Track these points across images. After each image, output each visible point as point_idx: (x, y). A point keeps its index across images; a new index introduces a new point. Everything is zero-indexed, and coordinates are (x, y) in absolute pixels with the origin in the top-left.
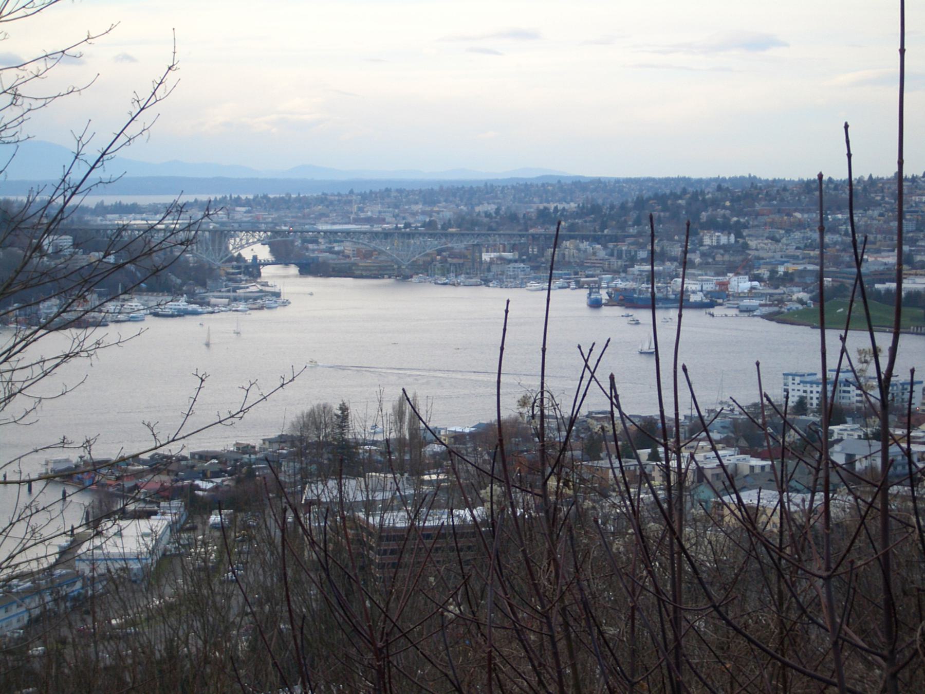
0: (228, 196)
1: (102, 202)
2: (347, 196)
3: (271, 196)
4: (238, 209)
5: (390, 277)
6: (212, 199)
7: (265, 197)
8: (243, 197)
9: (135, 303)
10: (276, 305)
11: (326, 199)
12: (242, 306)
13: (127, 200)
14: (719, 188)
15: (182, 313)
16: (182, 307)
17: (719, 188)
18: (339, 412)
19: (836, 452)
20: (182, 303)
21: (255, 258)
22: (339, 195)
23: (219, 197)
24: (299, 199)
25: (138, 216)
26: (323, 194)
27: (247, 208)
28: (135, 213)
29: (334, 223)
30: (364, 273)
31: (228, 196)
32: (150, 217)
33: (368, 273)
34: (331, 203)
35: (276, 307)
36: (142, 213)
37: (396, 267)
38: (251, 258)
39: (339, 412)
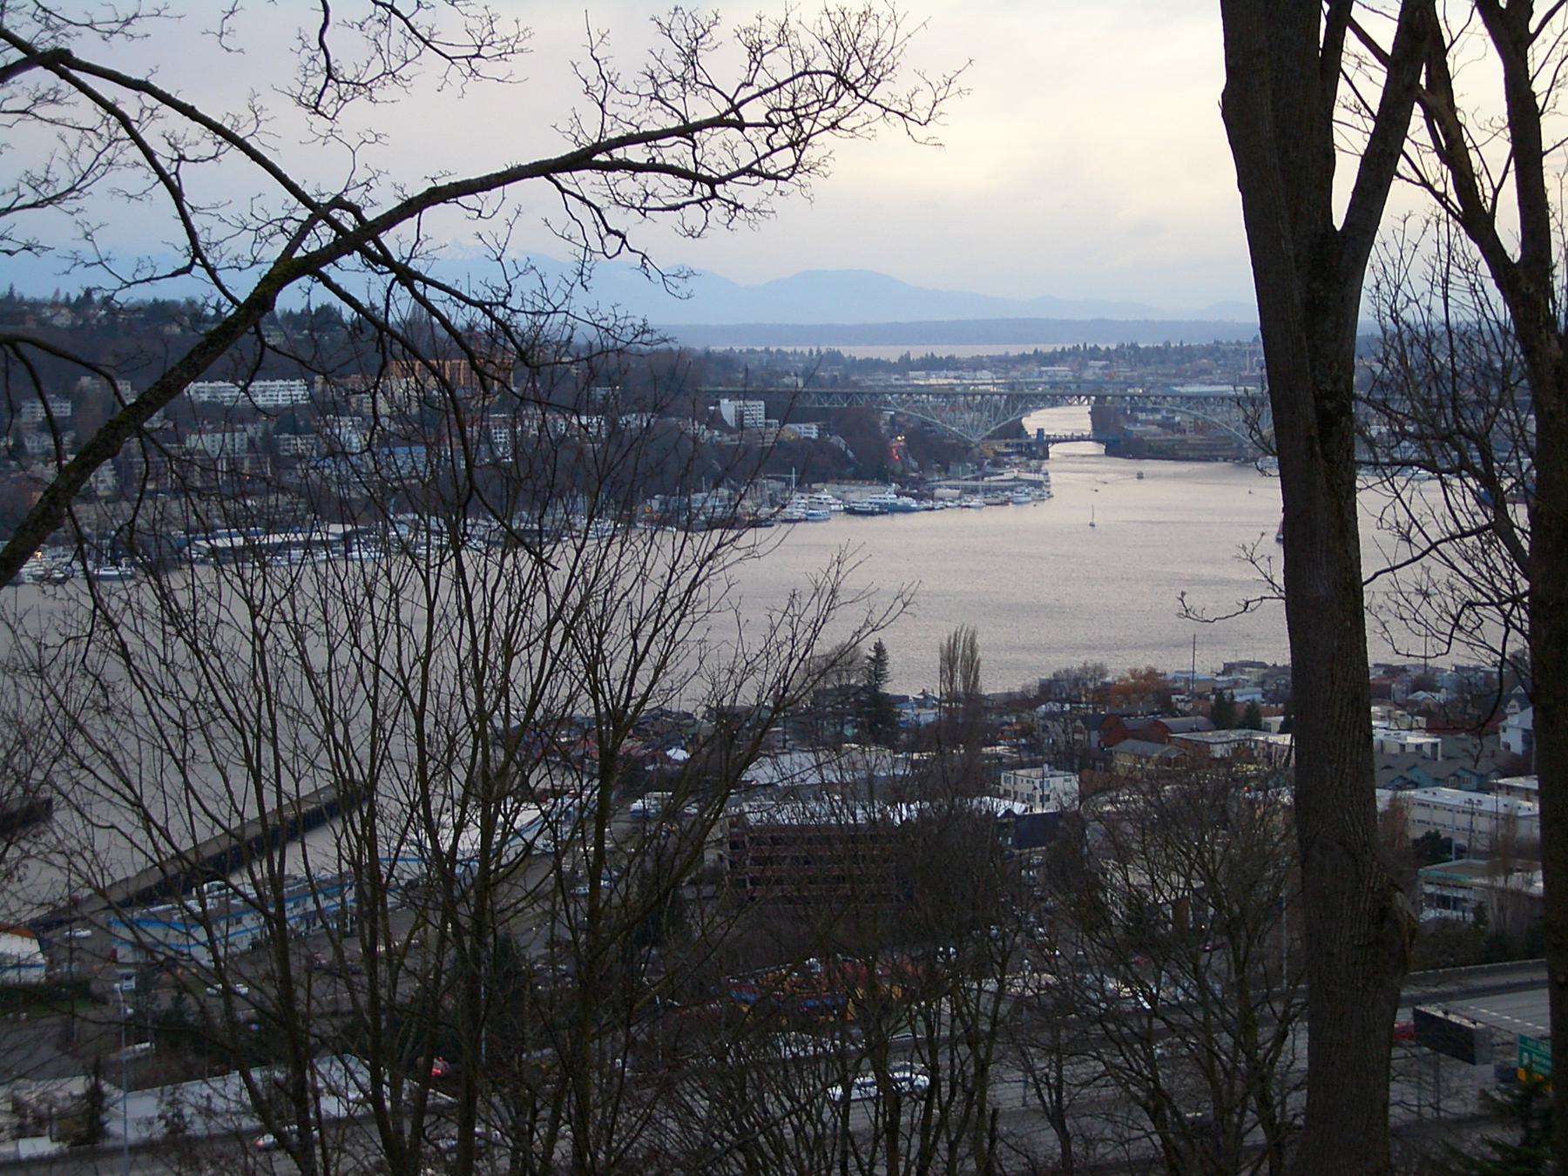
0: (1081, 346)
1: (908, 354)
2: (1250, 345)
3: (1142, 346)
4: (1092, 363)
5: (1225, 460)
6: (1059, 350)
7: (1134, 347)
8: (1103, 348)
9: (826, 494)
10: (1029, 499)
11: (1217, 348)
12: (976, 501)
13: (942, 352)
14: (656, 379)
15: (891, 510)
16: (889, 501)
17: (656, 379)
18: (873, 655)
19: (1511, 727)
20: (889, 496)
21: (1040, 432)
22: (1239, 343)
23: (1068, 346)
24: (1180, 350)
25: (952, 374)
26: (1217, 342)
27: (1104, 363)
28: (948, 369)
29: (1212, 383)
30: (1191, 454)
31: (1081, 346)
32: (965, 374)
33: (1196, 454)
34: (1224, 355)
35: (1028, 502)
36: (957, 369)
37: (1235, 445)
38: (1035, 432)
39: (873, 655)
